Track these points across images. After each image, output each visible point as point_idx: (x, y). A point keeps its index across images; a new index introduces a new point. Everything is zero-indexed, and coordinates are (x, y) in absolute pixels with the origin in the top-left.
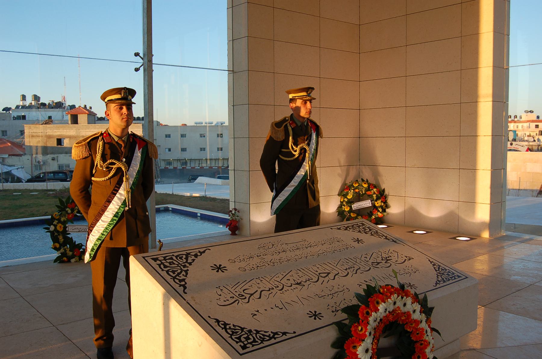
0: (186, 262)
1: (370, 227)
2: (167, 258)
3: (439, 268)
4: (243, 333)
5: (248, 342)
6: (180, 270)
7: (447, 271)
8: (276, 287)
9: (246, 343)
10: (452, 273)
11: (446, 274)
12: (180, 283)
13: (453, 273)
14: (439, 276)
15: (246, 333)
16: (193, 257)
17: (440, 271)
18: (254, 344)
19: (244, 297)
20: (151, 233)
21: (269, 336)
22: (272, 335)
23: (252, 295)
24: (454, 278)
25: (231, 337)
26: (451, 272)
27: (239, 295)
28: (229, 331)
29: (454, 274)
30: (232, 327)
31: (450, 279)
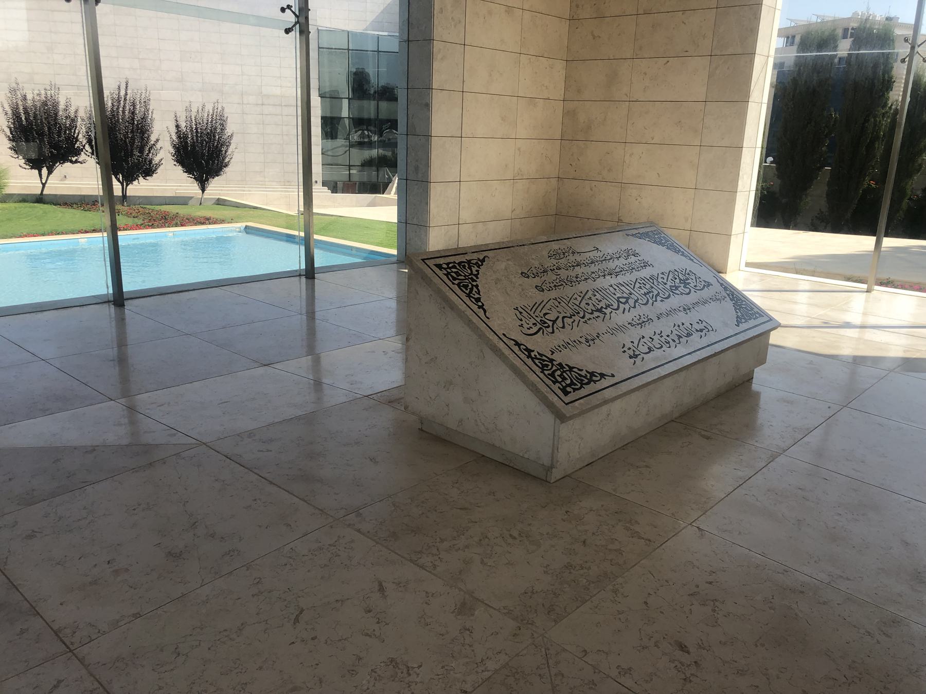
0: (471, 274)
1: (552, 381)
7: (456, 282)
10: (449, 276)
11: (462, 276)
13: (447, 275)
14: (474, 275)
16: (533, 354)
17: (470, 283)
19: (546, 325)
24: (450, 265)
27: (541, 320)
29: (446, 273)
31: (457, 265)
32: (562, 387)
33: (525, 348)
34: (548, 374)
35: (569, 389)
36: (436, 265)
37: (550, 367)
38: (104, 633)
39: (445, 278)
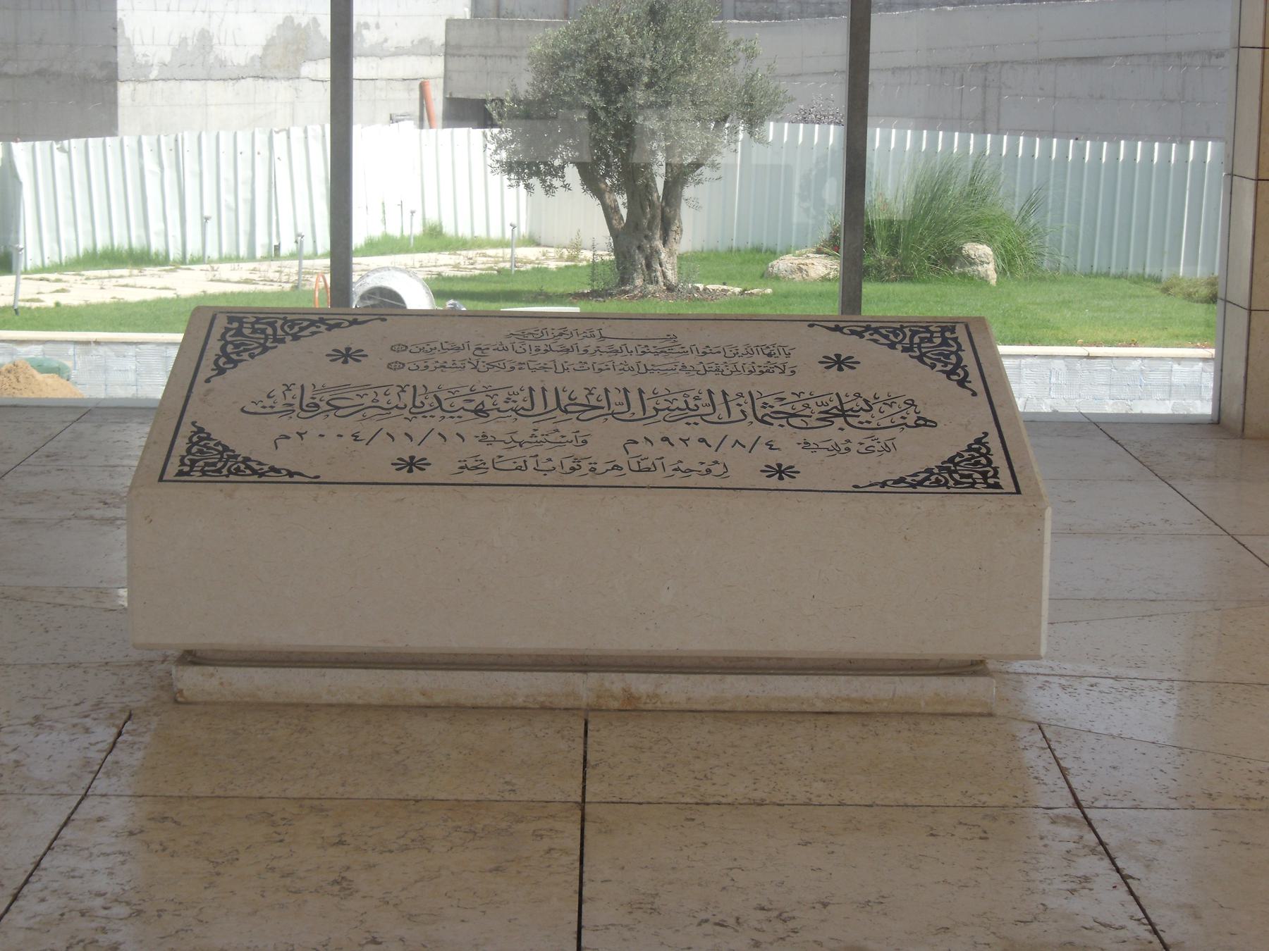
11: (217, 463)
32: (245, 320)
33: (342, 326)
34: (276, 322)
35: (235, 325)
37: (286, 328)
38: (1024, 804)
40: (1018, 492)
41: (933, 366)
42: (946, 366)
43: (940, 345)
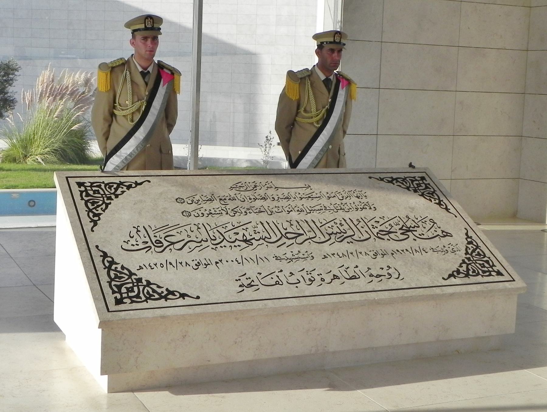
0: (468, 265)
2: (95, 185)
3: (474, 251)
4: (422, 191)
5: (128, 295)
6: (102, 202)
7: (486, 259)
8: (212, 239)
9: (421, 182)
11: (480, 264)
12: (94, 218)
13: (494, 265)
14: (466, 263)
15: (133, 283)
16: (125, 188)
18: (413, 179)
20: (100, 152)
21: (397, 181)
22: (394, 182)
23: (173, 243)
24: (488, 274)
25: (435, 191)
26: (490, 262)
28: (112, 274)
30: (433, 200)
36: (502, 275)
39: (496, 263)
40: (67, 178)
41: (123, 267)
42: (116, 268)
43: (122, 285)
